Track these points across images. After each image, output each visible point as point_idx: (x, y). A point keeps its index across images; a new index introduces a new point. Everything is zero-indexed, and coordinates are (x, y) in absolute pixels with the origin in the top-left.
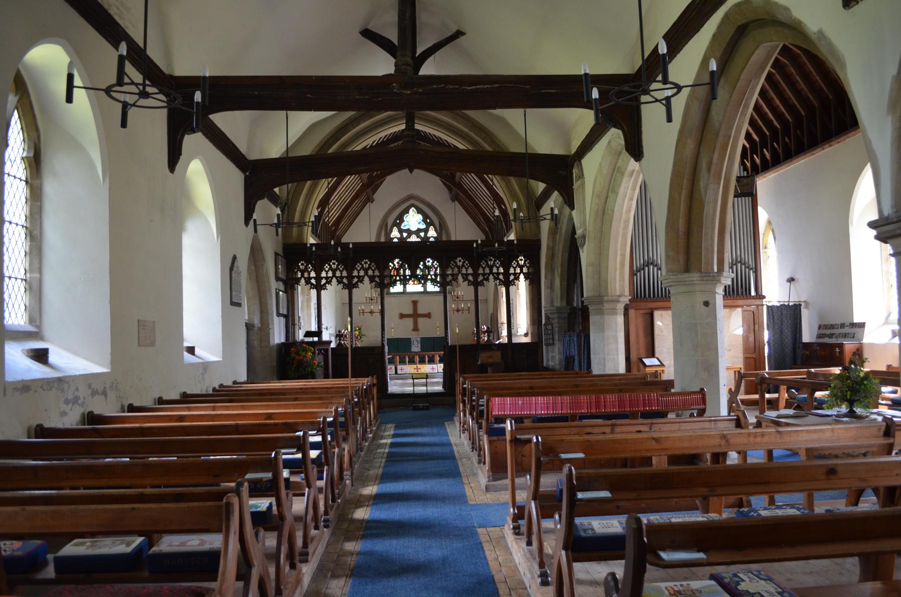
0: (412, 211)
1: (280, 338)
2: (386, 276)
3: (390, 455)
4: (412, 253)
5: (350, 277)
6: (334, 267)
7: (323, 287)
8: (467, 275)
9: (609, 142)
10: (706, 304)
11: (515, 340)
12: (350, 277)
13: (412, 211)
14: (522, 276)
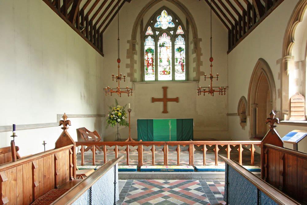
0: (164, 13)
13: (164, 13)
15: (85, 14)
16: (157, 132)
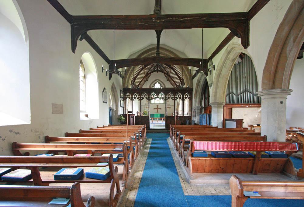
0: (157, 83)
1: (121, 112)
2: (150, 97)
3: (149, 153)
4: (158, 91)
5: (141, 97)
6: (136, 94)
7: (133, 100)
8: (172, 97)
9: (227, 48)
10: (281, 103)
11: (185, 115)
12: (141, 97)
13: (157, 83)
14: (187, 98)
15: (114, 193)
16: (155, 117)
